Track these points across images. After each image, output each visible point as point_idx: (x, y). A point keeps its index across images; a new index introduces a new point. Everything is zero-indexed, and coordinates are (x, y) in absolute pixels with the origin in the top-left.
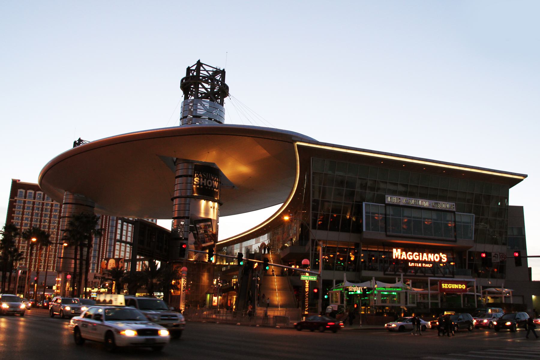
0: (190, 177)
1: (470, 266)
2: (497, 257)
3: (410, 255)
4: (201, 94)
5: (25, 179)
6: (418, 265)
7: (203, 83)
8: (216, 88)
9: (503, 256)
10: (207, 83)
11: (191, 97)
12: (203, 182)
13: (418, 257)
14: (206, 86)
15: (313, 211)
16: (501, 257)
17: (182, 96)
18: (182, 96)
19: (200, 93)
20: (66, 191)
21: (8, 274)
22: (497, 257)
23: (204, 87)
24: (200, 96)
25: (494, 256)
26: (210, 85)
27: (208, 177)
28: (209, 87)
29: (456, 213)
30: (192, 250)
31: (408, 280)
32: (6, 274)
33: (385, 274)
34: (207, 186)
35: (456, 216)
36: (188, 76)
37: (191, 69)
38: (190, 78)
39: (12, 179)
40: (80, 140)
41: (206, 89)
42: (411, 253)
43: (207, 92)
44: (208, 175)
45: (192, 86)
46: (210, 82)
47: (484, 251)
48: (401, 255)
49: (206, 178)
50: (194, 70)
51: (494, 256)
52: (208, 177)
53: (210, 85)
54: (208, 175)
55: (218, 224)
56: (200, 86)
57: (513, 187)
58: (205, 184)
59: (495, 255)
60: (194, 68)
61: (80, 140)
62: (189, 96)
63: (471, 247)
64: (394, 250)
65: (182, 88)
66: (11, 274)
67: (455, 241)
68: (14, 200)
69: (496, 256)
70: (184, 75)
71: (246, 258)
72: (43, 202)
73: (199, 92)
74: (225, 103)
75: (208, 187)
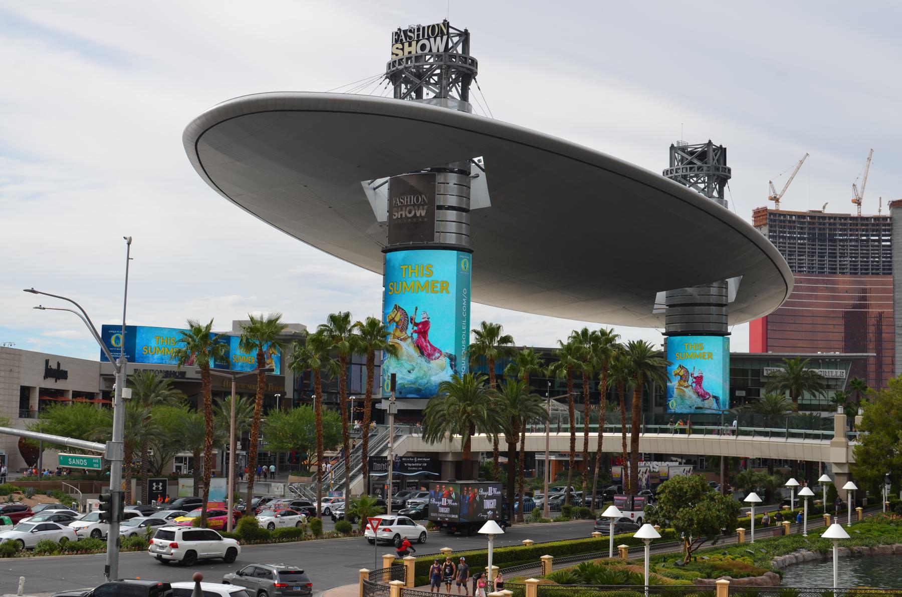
27: (407, 202)
34: (406, 217)
44: (407, 198)
52: (407, 202)
54: (407, 198)
58: (404, 216)
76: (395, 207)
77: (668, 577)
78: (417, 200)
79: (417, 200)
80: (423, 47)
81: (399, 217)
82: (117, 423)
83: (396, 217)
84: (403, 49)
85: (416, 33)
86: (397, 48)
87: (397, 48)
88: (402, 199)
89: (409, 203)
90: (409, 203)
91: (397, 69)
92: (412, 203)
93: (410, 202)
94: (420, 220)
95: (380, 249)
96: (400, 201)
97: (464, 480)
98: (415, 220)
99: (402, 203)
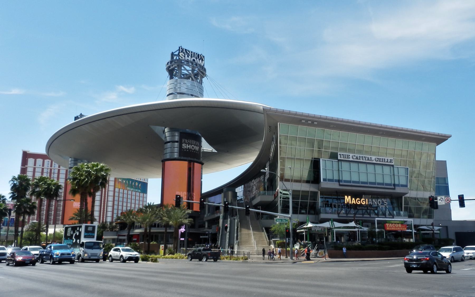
0: (176, 142)
1: (406, 209)
2: (442, 201)
3: (358, 200)
4: (183, 75)
5: (32, 150)
6: (362, 208)
7: (185, 65)
8: (196, 70)
9: (448, 199)
10: (189, 66)
11: (175, 77)
12: (189, 147)
13: (364, 202)
14: (188, 68)
15: (22, 166)
16: (446, 200)
17: (168, 77)
18: (168, 77)
19: (182, 74)
20: (70, 158)
21: (20, 229)
22: (442, 201)
23: (185, 69)
24: (183, 76)
25: (440, 200)
26: (191, 67)
27: (192, 143)
28: (191, 69)
29: (394, 166)
30: (144, 199)
31: (58, 182)
32: (18, 229)
33: (339, 216)
35: (394, 168)
36: (173, 60)
37: (174, 54)
38: (174, 61)
39: (22, 150)
40: (81, 115)
41: (187, 71)
42: (359, 199)
43: (188, 73)
45: (176, 69)
46: (190, 65)
47: (431, 195)
48: (351, 201)
49: (190, 144)
50: (177, 55)
51: (440, 200)
52: (192, 143)
53: (191, 67)
54: (192, 141)
55: (202, 180)
56: (183, 68)
57: (444, 142)
59: (441, 199)
60: (177, 53)
61: (81, 115)
62: (174, 77)
63: (406, 193)
64: (346, 197)
65: (167, 70)
66: (22, 229)
67: (394, 189)
68: (25, 167)
69: (442, 199)
70: (169, 59)
71: (377, 232)
72: (43, 167)
73: (182, 73)
74: (203, 83)
75: (192, 150)
76: (184, 143)
84: (186, 146)
87: (184, 147)
98: (195, 152)
99: (189, 142)
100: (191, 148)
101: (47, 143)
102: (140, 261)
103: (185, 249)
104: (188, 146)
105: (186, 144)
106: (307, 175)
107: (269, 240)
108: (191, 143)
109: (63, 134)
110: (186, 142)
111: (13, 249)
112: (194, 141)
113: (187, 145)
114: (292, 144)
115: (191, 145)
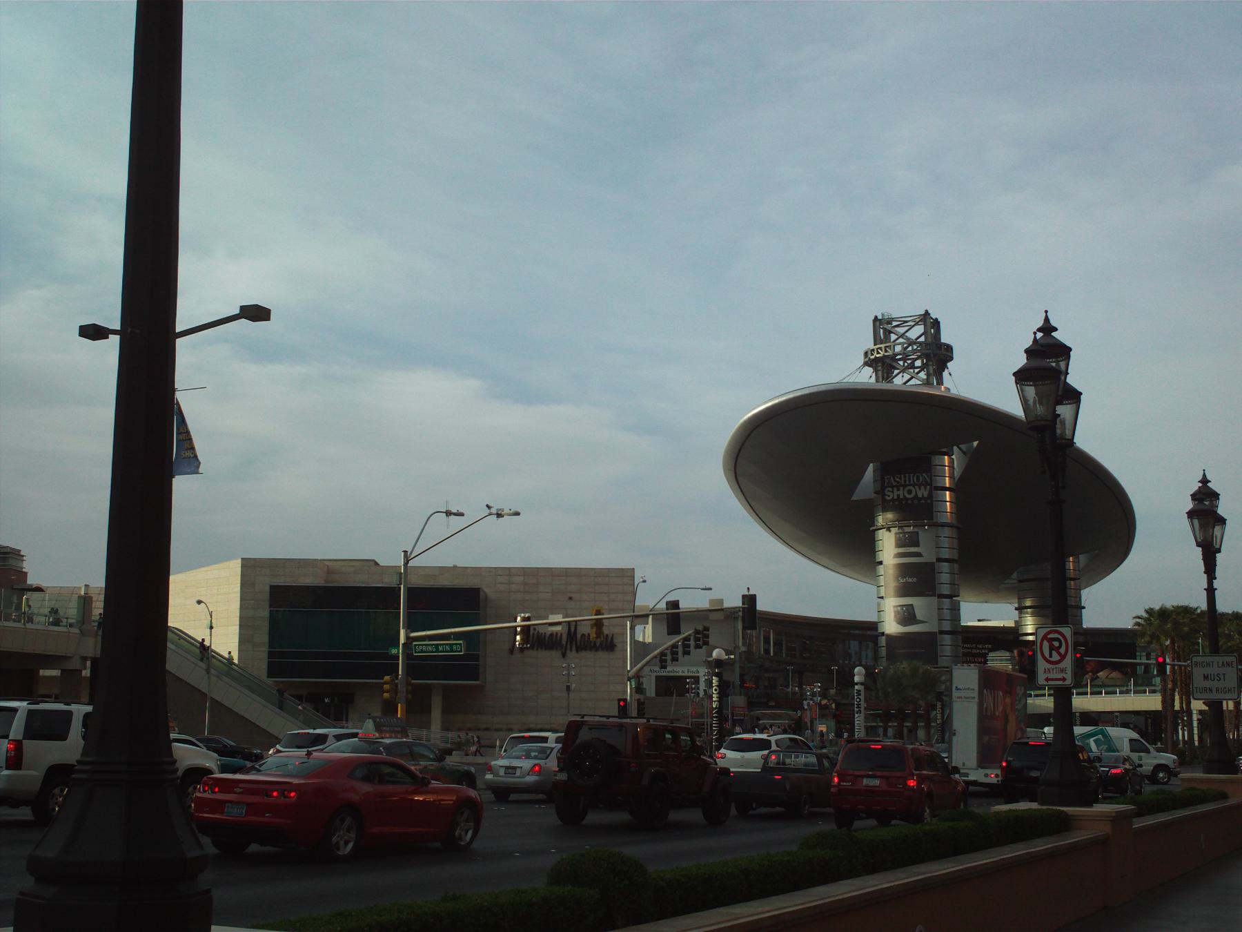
27: (905, 481)
34: (905, 498)
44: (905, 477)
52: (905, 481)
54: (905, 477)
58: (901, 497)
77: (845, 704)
78: (918, 480)
79: (918, 480)
80: (910, 492)
81: (895, 497)
82: (1196, 810)
83: (891, 497)
84: (893, 492)
85: (903, 479)
86: (889, 496)
87: (889, 496)
88: (897, 477)
89: (907, 483)
90: (907, 483)
91: (876, 357)
92: (912, 482)
93: (910, 481)
94: (923, 501)
95: (884, 563)
96: (895, 481)
97: (490, 624)
99: (898, 482)
100: (904, 496)
101: (1135, 528)
102: (935, 561)
103: (1076, 562)
104: (896, 493)
105: (893, 487)
106: (1138, 735)
107: (400, 588)
108: (903, 483)
109: (755, 512)
110: (892, 483)
111: (898, 553)
112: (912, 475)
113: (895, 489)
114: (208, 630)
115: (904, 486)
